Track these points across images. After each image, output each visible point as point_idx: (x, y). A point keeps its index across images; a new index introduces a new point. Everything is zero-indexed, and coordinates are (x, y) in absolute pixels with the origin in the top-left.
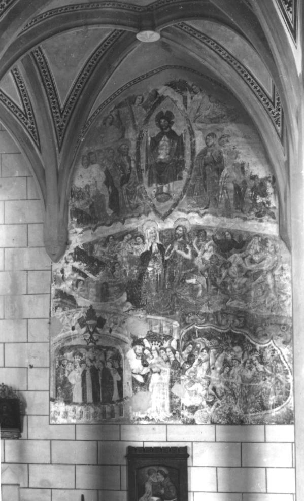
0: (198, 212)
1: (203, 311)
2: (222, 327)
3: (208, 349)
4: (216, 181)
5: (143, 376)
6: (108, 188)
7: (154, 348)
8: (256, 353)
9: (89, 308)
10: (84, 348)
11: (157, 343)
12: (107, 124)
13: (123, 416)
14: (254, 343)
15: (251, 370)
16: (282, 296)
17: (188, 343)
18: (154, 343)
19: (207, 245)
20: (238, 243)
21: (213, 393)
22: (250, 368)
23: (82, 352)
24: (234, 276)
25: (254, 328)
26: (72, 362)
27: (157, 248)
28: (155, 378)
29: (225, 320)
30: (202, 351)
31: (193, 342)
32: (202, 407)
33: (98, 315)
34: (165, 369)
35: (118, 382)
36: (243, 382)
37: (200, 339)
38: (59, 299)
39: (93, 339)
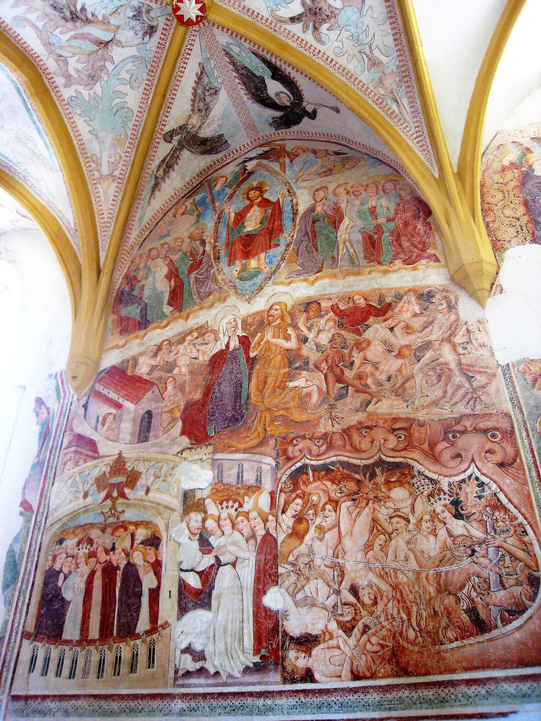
0: (305, 280)
1: (321, 430)
2: (363, 455)
3: (336, 504)
4: (331, 235)
5: (200, 574)
6: (170, 281)
7: (224, 515)
8: (442, 496)
9: (117, 456)
10: (97, 528)
11: (231, 503)
12: (178, 215)
13: (153, 667)
14: (435, 477)
15: (436, 536)
16: (478, 377)
17: (294, 495)
18: (225, 504)
19: (323, 321)
20: (379, 307)
21: (351, 599)
22: (434, 533)
23: (93, 536)
24: (377, 360)
25: (429, 445)
26: (73, 557)
27: (237, 342)
28: (224, 579)
29: (368, 439)
30: (323, 509)
31: (304, 493)
32: (327, 637)
33: (129, 466)
34: (247, 555)
35: (151, 591)
36: (421, 567)
37: (318, 483)
38: (73, 449)
39: (116, 510)
